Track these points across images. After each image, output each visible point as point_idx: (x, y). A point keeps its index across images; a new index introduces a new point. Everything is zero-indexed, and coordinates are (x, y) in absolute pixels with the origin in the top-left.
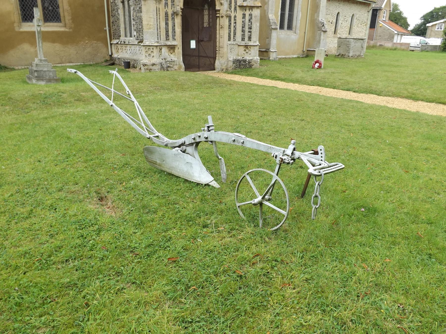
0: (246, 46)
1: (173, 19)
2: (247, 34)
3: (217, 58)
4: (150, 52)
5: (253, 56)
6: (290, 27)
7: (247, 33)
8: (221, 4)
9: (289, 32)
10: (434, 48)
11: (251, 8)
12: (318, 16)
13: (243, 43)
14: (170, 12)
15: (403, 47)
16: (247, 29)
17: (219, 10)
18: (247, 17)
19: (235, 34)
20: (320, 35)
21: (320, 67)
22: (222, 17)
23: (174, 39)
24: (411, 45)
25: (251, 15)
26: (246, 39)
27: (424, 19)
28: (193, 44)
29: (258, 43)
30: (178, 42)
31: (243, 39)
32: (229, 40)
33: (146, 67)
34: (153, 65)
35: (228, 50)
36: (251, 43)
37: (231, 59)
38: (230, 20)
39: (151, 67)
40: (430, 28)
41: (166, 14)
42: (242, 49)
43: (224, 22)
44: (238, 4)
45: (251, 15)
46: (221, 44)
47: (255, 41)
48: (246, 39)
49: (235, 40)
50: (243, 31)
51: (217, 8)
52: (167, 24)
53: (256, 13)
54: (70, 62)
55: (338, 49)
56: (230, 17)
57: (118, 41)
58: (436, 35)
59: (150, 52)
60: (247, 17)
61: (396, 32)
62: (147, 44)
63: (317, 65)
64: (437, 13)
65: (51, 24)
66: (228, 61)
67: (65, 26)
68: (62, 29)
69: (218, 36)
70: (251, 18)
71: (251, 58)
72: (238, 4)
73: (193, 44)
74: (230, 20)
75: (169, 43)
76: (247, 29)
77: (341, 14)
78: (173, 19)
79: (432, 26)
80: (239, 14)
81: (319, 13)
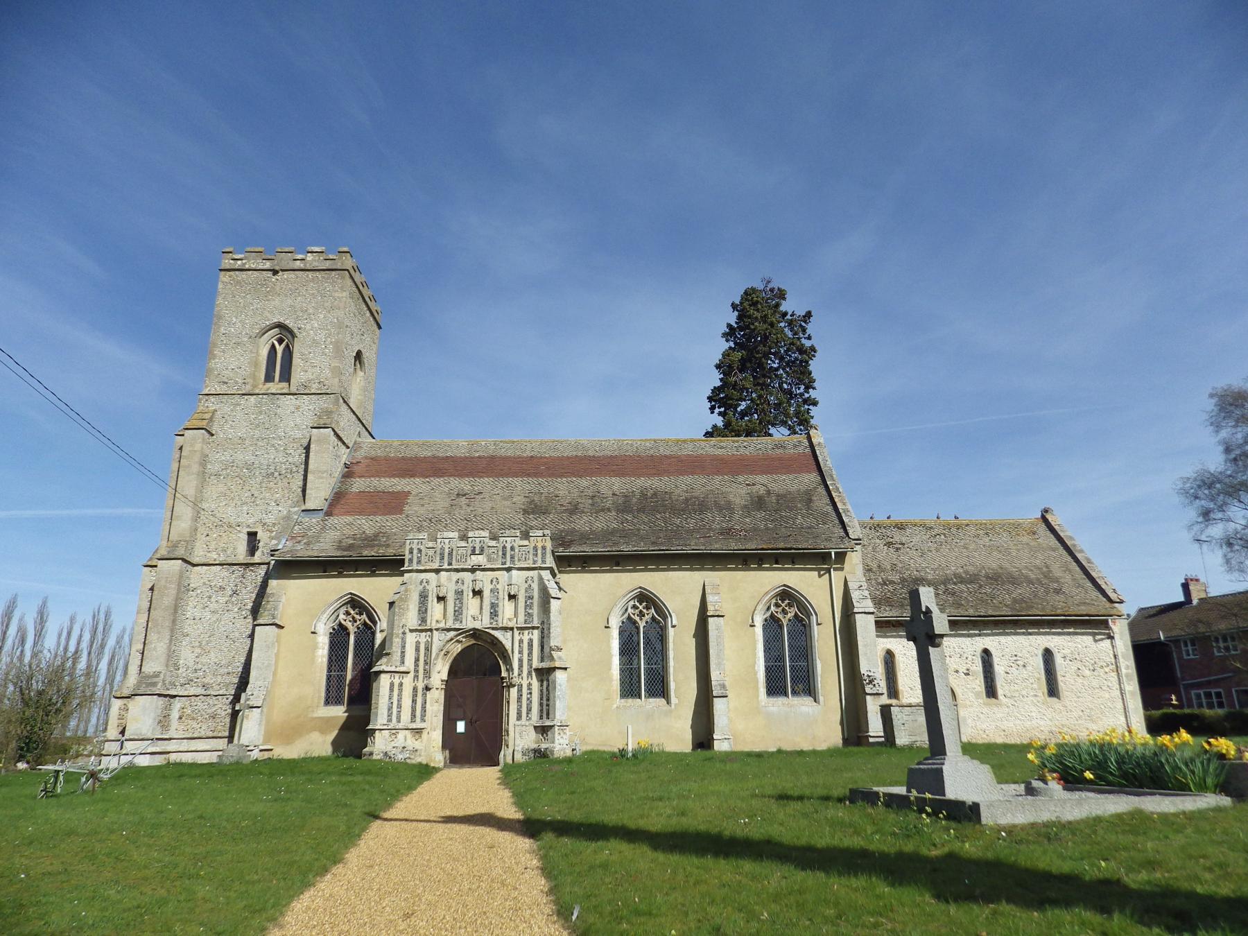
1: (424, 695)
6: (806, 685)
14: (420, 685)
19: (529, 710)
23: (423, 720)
28: (461, 727)
32: (519, 717)
41: (415, 689)
52: (414, 701)
73: (461, 727)
75: (414, 726)
76: (545, 702)
78: (424, 695)
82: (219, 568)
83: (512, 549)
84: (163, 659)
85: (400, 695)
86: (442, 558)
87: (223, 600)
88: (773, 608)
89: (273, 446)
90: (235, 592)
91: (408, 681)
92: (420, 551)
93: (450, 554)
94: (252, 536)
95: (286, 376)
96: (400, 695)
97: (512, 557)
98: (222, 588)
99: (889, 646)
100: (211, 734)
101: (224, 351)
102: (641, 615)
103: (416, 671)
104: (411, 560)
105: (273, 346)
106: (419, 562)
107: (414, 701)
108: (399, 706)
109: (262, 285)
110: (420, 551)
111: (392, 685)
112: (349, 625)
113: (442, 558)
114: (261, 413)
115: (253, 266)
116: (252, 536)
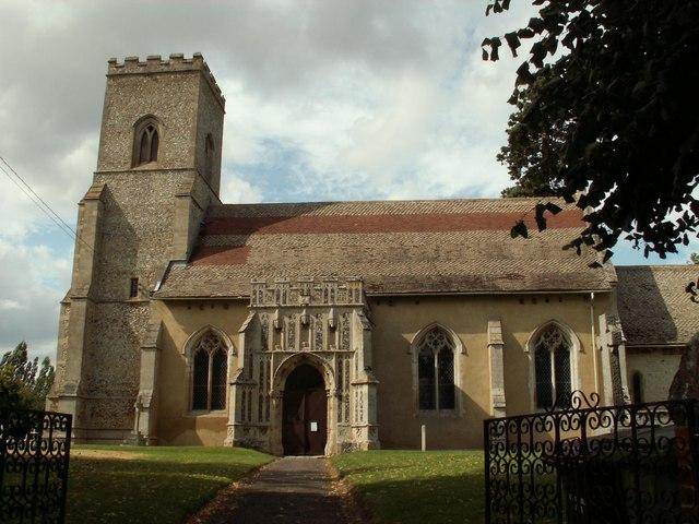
1: (268, 402)
9: (446, 413)
23: (268, 420)
31: (357, 420)
32: (340, 420)
41: (261, 397)
51: (327, 388)
52: (261, 406)
83: (333, 291)
84: (79, 371)
85: (250, 401)
86: (278, 299)
88: (543, 338)
91: (255, 391)
92: (261, 293)
93: (285, 295)
95: (153, 158)
96: (250, 401)
97: (333, 297)
99: (636, 368)
102: (551, 342)
103: (261, 384)
104: (255, 300)
105: (145, 133)
106: (261, 302)
107: (261, 406)
108: (250, 409)
110: (261, 293)
111: (244, 393)
112: (208, 349)
113: (278, 299)
116: (134, 281)
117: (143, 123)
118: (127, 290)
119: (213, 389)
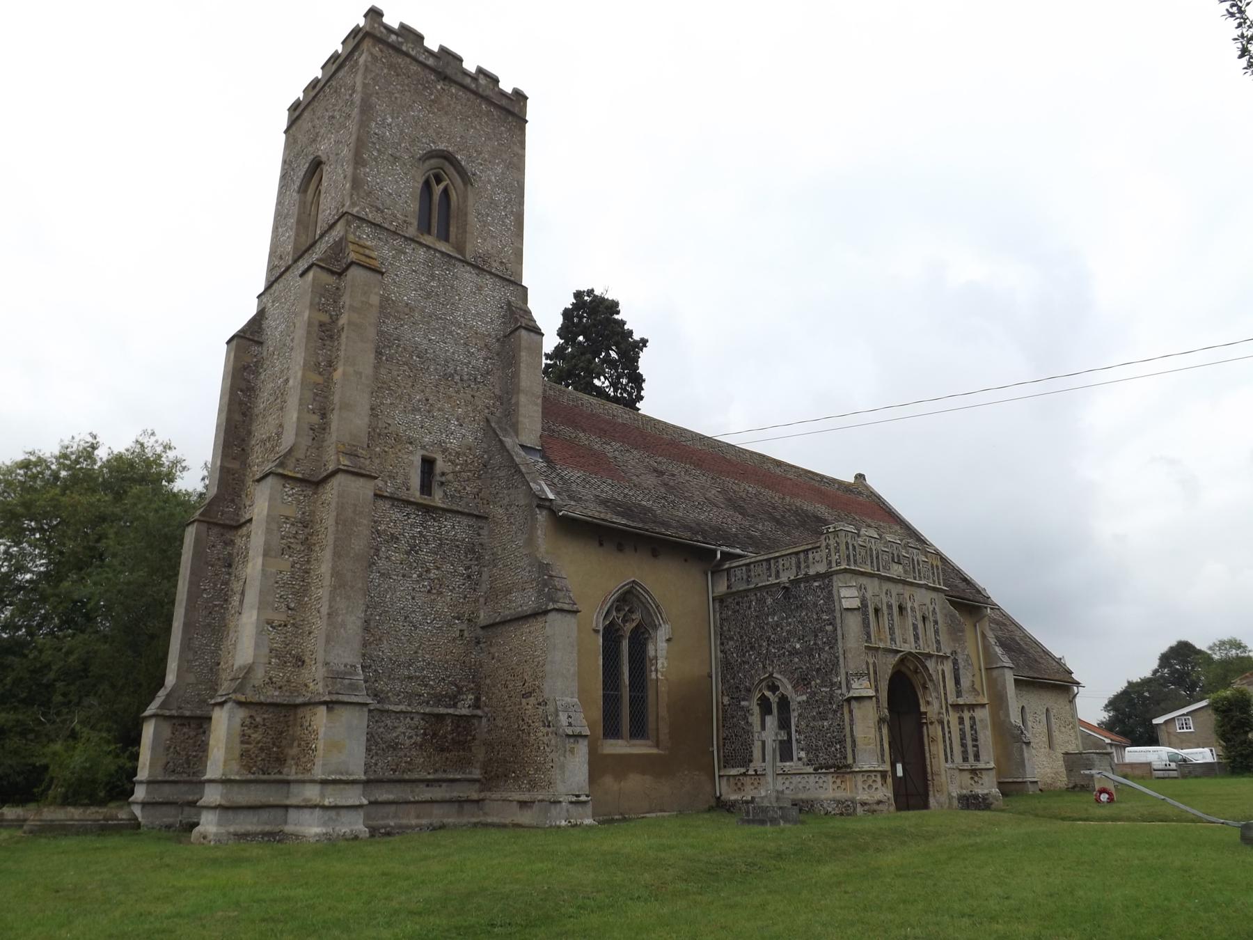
0: (974, 772)
2: (970, 749)
3: (931, 793)
4: (870, 782)
5: (988, 787)
7: (970, 748)
8: (928, 703)
10: (1207, 770)
11: (972, 707)
12: (1008, 715)
13: (967, 766)
15: (1138, 772)
16: (969, 743)
17: (925, 713)
18: (967, 723)
20: (1022, 750)
21: (1111, 800)
22: (932, 723)
24: (477, 786)
25: (972, 718)
26: (971, 758)
27: (1115, 709)
29: (992, 765)
30: (887, 767)
31: (965, 759)
33: (866, 808)
34: (879, 802)
35: (949, 779)
36: (981, 765)
37: (954, 794)
38: (943, 729)
39: (875, 807)
40: (1163, 727)
42: (967, 776)
43: (936, 731)
44: (950, 702)
45: (972, 718)
46: (935, 769)
47: (988, 760)
48: (971, 758)
49: (953, 762)
50: (963, 745)
51: (923, 709)
53: (983, 715)
54: (661, 811)
55: (1068, 776)
56: (941, 722)
57: (743, 770)
58: (1182, 742)
59: (870, 782)
60: (967, 723)
61: (1108, 741)
62: (866, 768)
63: (1104, 797)
64: (1140, 695)
65: (638, 742)
66: (950, 797)
67: (657, 746)
68: (655, 751)
69: (927, 755)
70: (975, 723)
71: (986, 791)
72: (950, 702)
74: (943, 729)
76: (969, 743)
77: (1027, 710)
79: (1166, 722)
80: (953, 718)
81: (1007, 710)
82: (388, 505)
87: (396, 557)
89: (451, 333)
90: (413, 547)
94: (428, 463)
98: (394, 538)
100: (389, 775)
101: (375, 159)
109: (425, 88)
114: (433, 277)
115: (413, 53)
117: (433, 161)
118: (415, 480)
119: (632, 701)
